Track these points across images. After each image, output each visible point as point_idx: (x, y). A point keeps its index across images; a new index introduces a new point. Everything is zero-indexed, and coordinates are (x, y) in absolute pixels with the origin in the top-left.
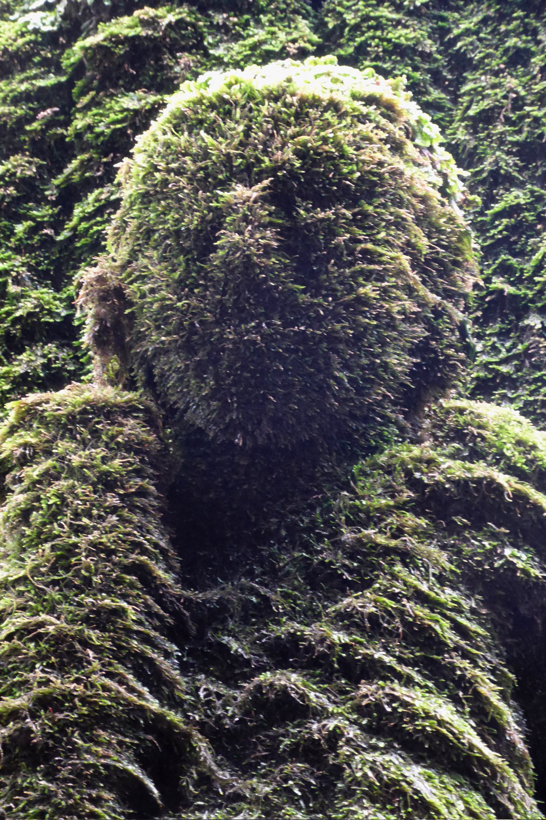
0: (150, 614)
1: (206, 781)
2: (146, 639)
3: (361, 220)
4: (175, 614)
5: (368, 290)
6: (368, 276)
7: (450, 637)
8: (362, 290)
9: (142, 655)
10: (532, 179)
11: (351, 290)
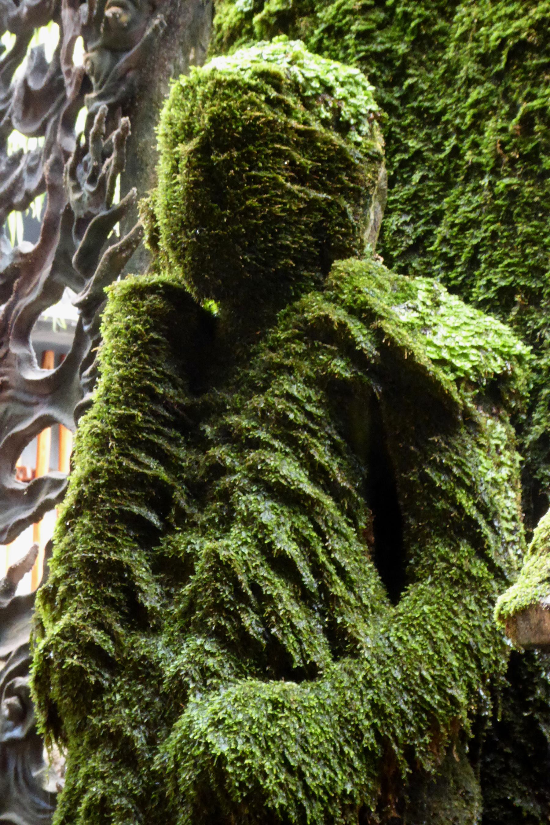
0: (154, 414)
1: (181, 514)
2: (150, 431)
3: (247, 157)
4: (174, 413)
5: (252, 202)
6: (254, 193)
7: (301, 419)
8: (248, 202)
9: (148, 440)
10: (489, 79)
11: (243, 203)
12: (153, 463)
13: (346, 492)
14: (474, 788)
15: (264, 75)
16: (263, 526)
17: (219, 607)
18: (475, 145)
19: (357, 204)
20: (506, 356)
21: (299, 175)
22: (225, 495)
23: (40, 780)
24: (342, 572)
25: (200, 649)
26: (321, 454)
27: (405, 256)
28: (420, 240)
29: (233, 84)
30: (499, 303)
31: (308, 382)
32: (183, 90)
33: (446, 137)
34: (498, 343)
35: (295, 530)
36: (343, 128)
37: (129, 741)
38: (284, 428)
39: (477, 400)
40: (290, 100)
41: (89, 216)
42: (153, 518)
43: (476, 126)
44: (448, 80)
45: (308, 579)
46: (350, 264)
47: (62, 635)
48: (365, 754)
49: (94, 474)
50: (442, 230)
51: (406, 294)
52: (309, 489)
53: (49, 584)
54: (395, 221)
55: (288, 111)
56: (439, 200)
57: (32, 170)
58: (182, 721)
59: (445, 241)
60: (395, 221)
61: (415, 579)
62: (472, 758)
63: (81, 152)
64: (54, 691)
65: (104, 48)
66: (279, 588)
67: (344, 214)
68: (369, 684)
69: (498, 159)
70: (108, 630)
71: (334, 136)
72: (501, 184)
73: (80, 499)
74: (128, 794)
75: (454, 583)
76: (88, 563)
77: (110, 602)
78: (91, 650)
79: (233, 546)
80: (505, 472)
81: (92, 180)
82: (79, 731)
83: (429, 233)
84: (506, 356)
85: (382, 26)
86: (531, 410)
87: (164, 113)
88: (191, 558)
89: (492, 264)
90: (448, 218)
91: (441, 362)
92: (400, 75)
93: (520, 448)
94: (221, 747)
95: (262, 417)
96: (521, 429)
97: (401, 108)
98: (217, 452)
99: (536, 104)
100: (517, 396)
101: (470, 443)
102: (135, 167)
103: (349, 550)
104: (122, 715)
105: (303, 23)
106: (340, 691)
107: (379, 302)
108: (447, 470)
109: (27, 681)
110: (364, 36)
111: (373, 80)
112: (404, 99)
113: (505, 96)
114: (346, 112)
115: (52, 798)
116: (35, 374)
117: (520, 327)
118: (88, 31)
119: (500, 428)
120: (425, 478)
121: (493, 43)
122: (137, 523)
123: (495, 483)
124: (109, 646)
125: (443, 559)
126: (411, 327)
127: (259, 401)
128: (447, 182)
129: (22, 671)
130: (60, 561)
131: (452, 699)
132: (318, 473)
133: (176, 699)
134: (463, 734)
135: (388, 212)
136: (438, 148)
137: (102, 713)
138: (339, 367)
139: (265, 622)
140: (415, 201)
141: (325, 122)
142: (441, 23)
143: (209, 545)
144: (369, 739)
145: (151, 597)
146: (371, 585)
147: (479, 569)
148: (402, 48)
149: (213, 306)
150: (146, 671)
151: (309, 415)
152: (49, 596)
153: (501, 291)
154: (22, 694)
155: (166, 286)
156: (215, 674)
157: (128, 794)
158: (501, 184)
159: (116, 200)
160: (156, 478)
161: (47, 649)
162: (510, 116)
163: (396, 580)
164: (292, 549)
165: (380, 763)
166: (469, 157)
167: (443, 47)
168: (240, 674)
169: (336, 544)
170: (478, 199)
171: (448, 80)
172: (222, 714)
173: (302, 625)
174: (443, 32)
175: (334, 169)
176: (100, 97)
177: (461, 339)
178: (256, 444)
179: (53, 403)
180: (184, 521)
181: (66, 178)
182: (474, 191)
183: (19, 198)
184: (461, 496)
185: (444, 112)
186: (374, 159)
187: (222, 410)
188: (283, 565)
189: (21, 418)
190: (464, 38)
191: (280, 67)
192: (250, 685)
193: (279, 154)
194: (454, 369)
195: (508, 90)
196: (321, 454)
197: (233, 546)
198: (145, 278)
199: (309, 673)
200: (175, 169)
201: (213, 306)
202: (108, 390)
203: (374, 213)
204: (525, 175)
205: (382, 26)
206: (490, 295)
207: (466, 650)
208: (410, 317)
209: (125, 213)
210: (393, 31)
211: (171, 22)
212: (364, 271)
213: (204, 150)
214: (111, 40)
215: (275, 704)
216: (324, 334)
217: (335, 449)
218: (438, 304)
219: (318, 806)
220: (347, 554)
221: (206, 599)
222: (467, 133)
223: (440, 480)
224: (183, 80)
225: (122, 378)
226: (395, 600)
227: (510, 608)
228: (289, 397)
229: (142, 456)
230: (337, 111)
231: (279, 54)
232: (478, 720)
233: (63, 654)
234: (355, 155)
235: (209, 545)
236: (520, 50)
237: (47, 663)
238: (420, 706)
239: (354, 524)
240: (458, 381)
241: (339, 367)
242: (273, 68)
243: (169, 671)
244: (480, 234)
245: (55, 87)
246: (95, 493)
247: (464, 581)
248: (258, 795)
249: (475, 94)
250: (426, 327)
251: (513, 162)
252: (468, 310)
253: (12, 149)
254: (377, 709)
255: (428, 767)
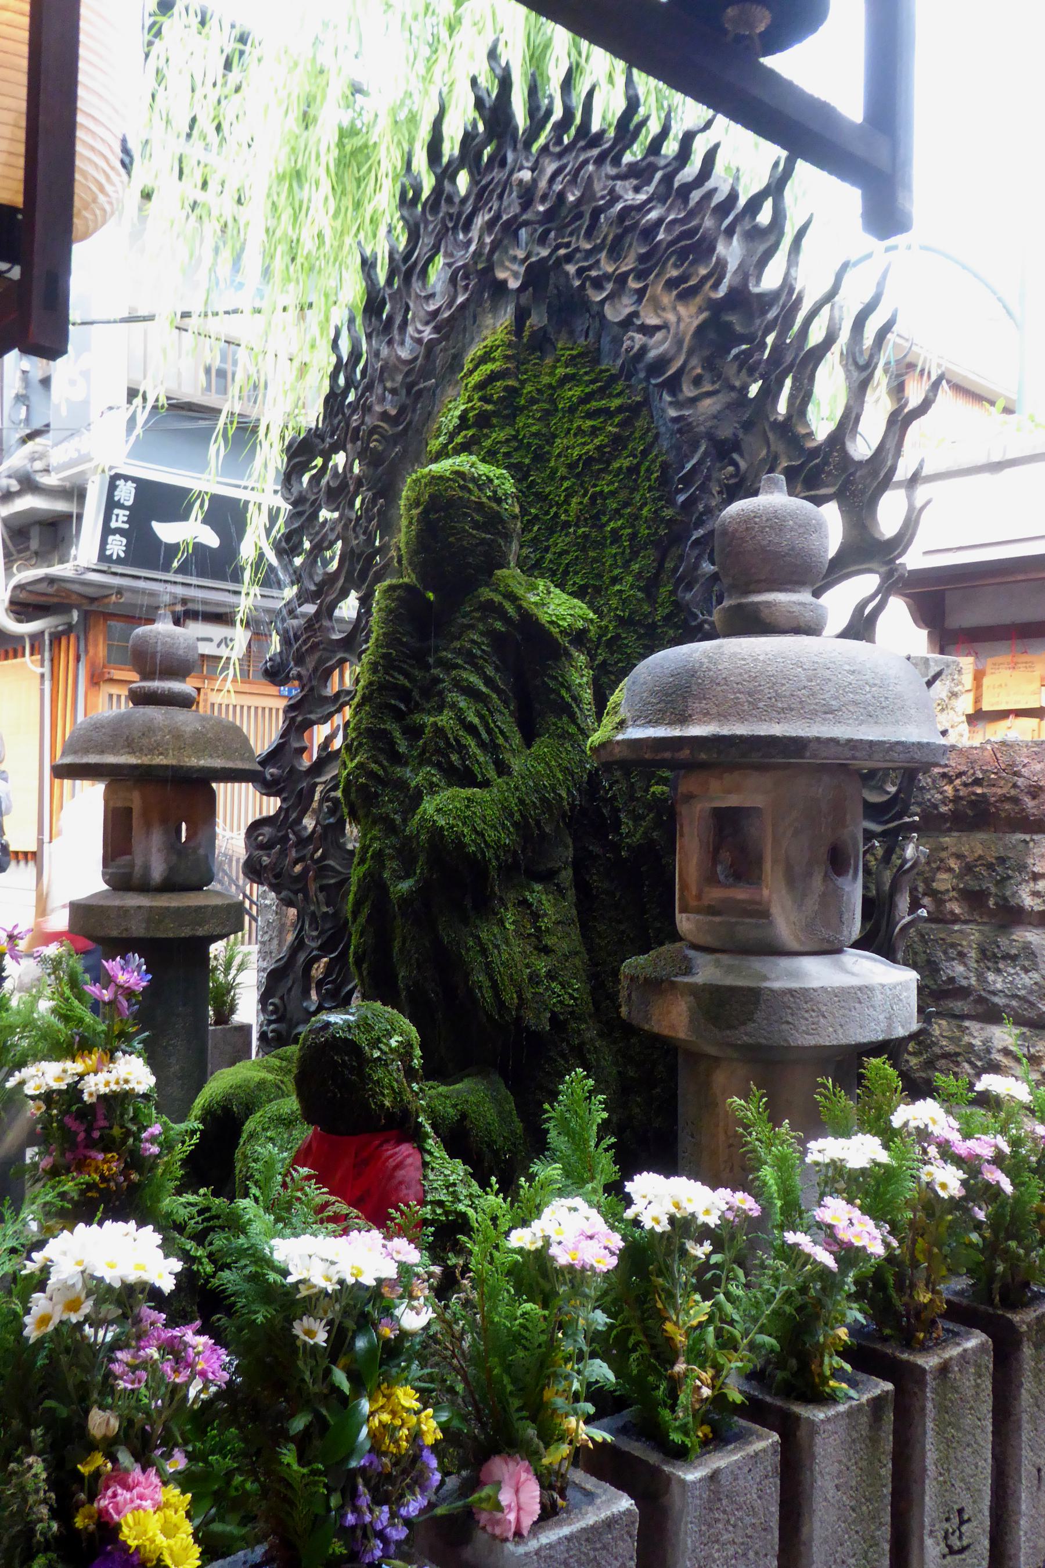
1: (417, 704)
5: (452, 539)
6: (453, 535)
7: (479, 653)
12: (401, 678)
13: (503, 691)
14: (569, 841)
15: (457, 473)
16: (460, 709)
17: (438, 751)
18: (566, 511)
19: (506, 542)
20: (585, 620)
21: (476, 525)
22: (440, 693)
23: (345, 844)
24: (502, 732)
25: (428, 773)
26: (490, 671)
27: (532, 569)
28: (537, 561)
29: (441, 478)
30: (580, 593)
31: (482, 634)
32: (414, 481)
33: (551, 507)
34: (581, 612)
35: (477, 711)
36: (499, 501)
37: (394, 820)
38: (470, 658)
39: (570, 642)
40: (471, 486)
41: (363, 553)
42: (402, 707)
43: (566, 501)
44: (552, 476)
45: (484, 735)
46: (505, 572)
47: (356, 767)
48: (515, 824)
49: (371, 684)
50: (549, 556)
51: (533, 587)
52: (484, 689)
53: (348, 741)
54: (525, 551)
55: (470, 491)
56: (547, 540)
57: (332, 529)
58: (421, 809)
59: (551, 561)
60: (525, 551)
61: (540, 736)
62: (568, 826)
63: (358, 518)
64: (353, 796)
65: (368, 465)
66: (470, 741)
67: (500, 546)
68: (517, 788)
69: (578, 518)
70: (381, 765)
71: (494, 505)
72: (580, 531)
73: (363, 697)
74: (392, 847)
75: (560, 737)
76: (368, 730)
77: (380, 750)
78: (371, 775)
79: (445, 719)
80: (585, 679)
81: (364, 533)
82: (367, 816)
83: (543, 557)
84: (585, 620)
85: (516, 449)
86: (597, 648)
87: (404, 493)
88: (423, 726)
89: (576, 573)
90: (553, 550)
91: (552, 622)
92: (525, 477)
93: (591, 668)
94: (442, 822)
95: (459, 652)
96: (592, 657)
97: (528, 493)
98: (435, 671)
99: (598, 489)
100: (590, 640)
101: (567, 664)
102: (387, 526)
103: (505, 721)
104: (388, 806)
105: (475, 448)
106: (502, 792)
107: (520, 591)
108: (555, 678)
109: (339, 794)
110: (507, 455)
111: (513, 477)
112: (529, 487)
113: (582, 485)
114: (500, 492)
115: (352, 853)
116: (336, 636)
117: (591, 606)
118: (361, 456)
119: (582, 657)
120: (544, 683)
121: (575, 457)
122: (395, 708)
123: (580, 685)
124: (381, 772)
125: (555, 724)
126: (536, 604)
127: (457, 644)
128: (551, 531)
129: (335, 788)
130: (354, 729)
131: (560, 795)
132: (488, 681)
133: (417, 798)
134: (565, 812)
135: (521, 547)
136: (547, 513)
137: (378, 807)
138: (498, 625)
139: (463, 759)
140: (535, 542)
141: (489, 498)
142: (547, 448)
143: (432, 719)
144: (517, 817)
145: (402, 748)
146: (517, 739)
147: (572, 729)
148: (527, 461)
149: (431, 596)
150: (401, 785)
151: (483, 651)
152: (348, 747)
153: (581, 587)
154: (336, 801)
155: (406, 584)
156: (437, 785)
157: (392, 847)
158: (580, 531)
159: (377, 544)
160: (403, 686)
161: (349, 774)
162: (584, 495)
163: (529, 737)
164: (476, 721)
165: (522, 827)
166: (563, 517)
167: (549, 460)
168: (450, 785)
169: (497, 716)
170: (568, 539)
171: (552, 476)
172: (440, 805)
173: (482, 759)
174: (548, 452)
175: (493, 522)
176: (368, 490)
177: (561, 611)
178: (456, 666)
179: (345, 651)
180: (418, 708)
181: (351, 532)
182: (566, 535)
183: (326, 544)
184: (563, 692)
185: (549, 494)
186: (515, 517)
187: (437, 650)
188: (471, 729)
189: (330, 659)
190: (559, 455)
191: (466, 468)
192: (456, 790)
193: (466, 514)
194: (559, 626)
195: (583, 482)
196: (490, 671)
197: (445, 719)
198: (394, 581)
199: (486, 784)
200: (411, 523)
201: (431, 596)
202: (377, 640)
203: (515, 546)
204: (592, 527)
205: (516, 449)
206: (575, 589)
207: (565, 770)
208: (534, 599)
209: (382, 550)
210: (522, 452)
211: (405, 450)
212: (511, 575)
213: (425, 512)
214: (371, 459)
215: (469, 799)
216: (490, 608)
217: (497, 669)
218: (549, 593)
219: (492, 851)
220: (504, 723)
221: (432, 747)
222: (562, 505)
223: (552, 684)
224: (414, 476)
225: (384, 634)
226: (529, 747)
227: (596, 743)
228: (473, 641)
229: (396, 674)
230: (495, 492)
231: (463, 462)
232: (572, 806)
233: (357, 777)
234: (506, 515)
235: (432, 719)
236: (589, 461)
237: (348, 782)
238: (543, 799)
239: (507, 708)
240: (561, 632)
241: (498, 625)
242: (461, 469)
243: (413, 784)
244: (569, 557)
245: (343, 486)
246: (372, 693)
247: (565, 736)
248: (461, 845)
249: (565, 485)
250: (544, 605)
251: (586, 519)
252: (565, 596)
253: (321, 520)
254: (521, 801)
255: (547, 830)
